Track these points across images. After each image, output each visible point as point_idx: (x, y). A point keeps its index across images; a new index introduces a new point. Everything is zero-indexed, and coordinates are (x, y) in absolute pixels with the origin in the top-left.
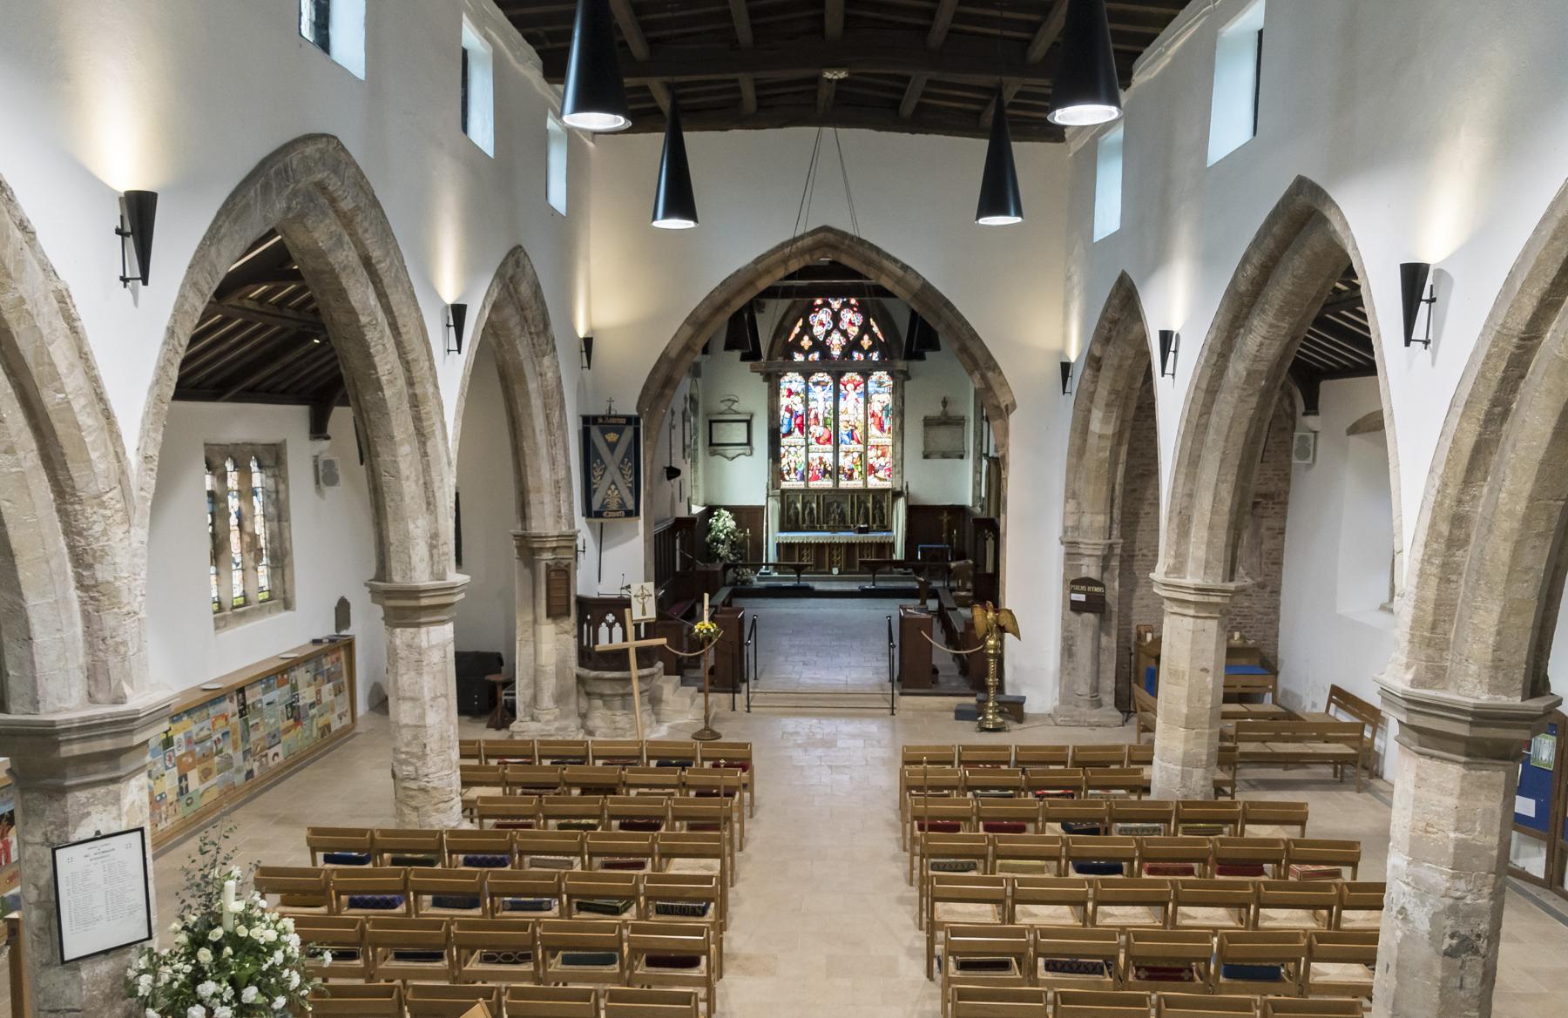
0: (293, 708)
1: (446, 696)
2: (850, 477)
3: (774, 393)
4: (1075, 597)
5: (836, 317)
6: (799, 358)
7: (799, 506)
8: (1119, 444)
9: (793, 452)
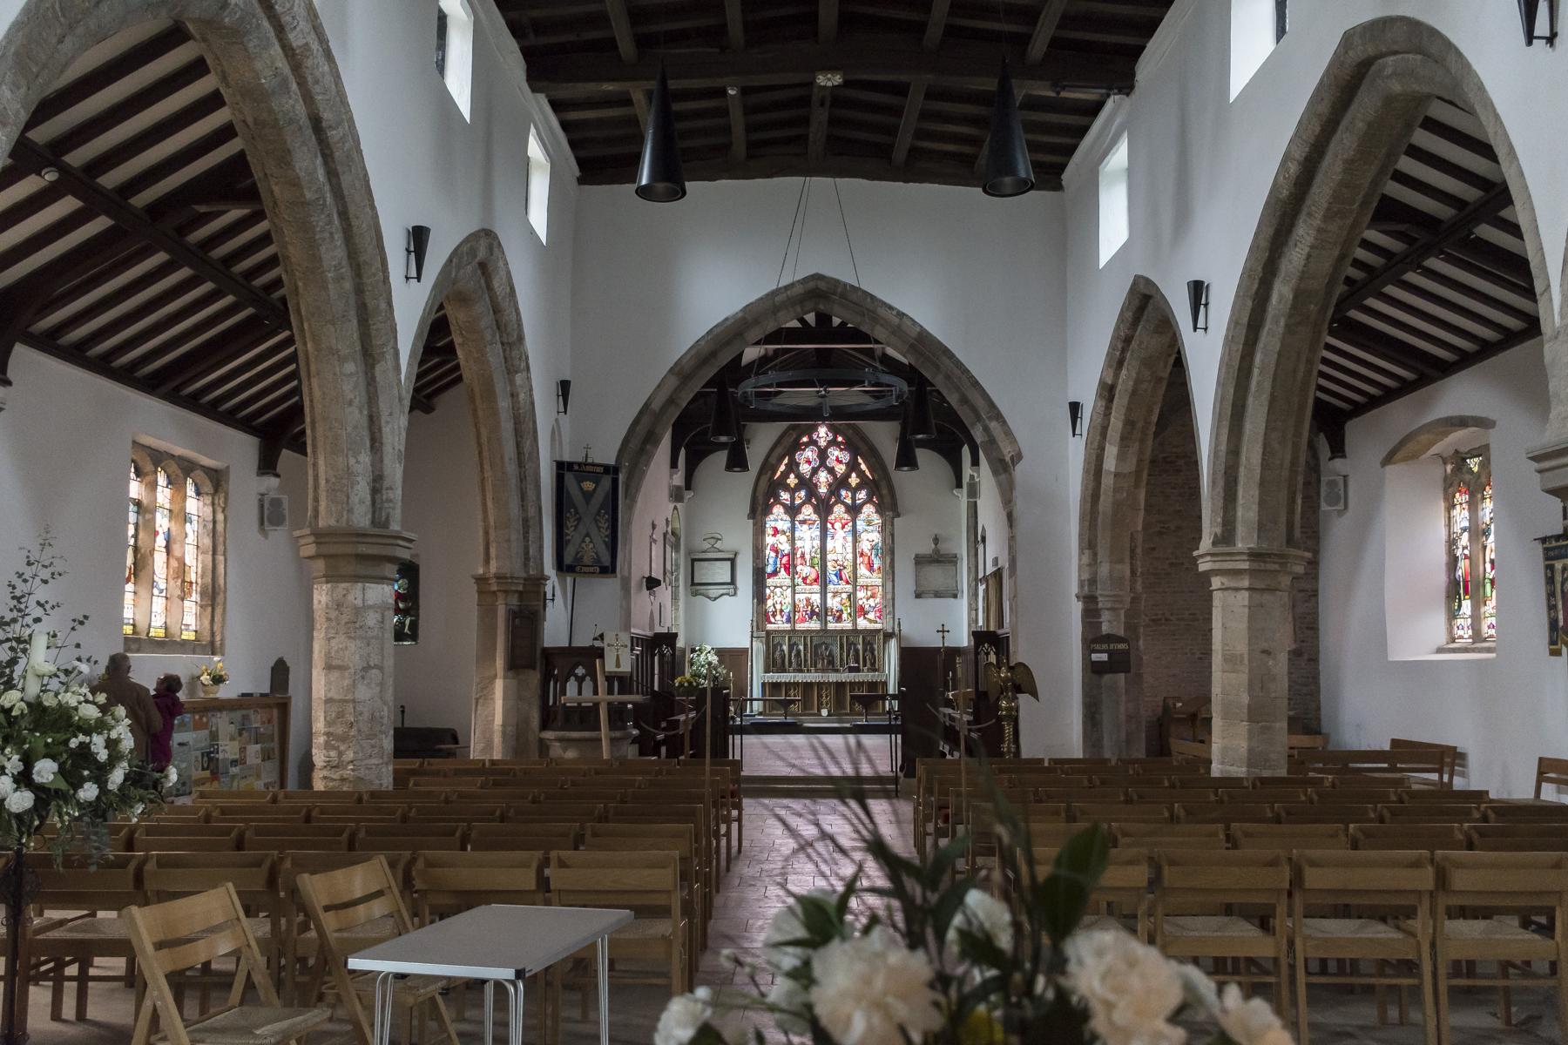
0: (210, 760)
1: (381, 668)
2: (839, 619)
3: (759, 531)
4: (1095, 657)
5: (823, 455)
6: (785, 496)
7: (785, 648)
8: (1137, 486)
9: (779, 595)
